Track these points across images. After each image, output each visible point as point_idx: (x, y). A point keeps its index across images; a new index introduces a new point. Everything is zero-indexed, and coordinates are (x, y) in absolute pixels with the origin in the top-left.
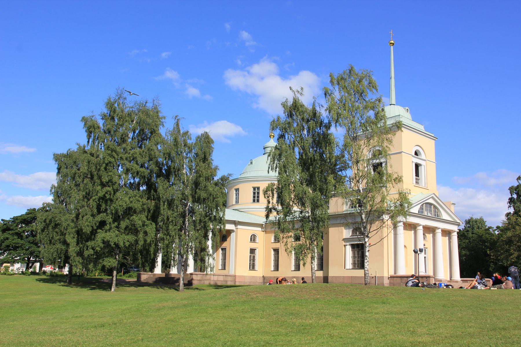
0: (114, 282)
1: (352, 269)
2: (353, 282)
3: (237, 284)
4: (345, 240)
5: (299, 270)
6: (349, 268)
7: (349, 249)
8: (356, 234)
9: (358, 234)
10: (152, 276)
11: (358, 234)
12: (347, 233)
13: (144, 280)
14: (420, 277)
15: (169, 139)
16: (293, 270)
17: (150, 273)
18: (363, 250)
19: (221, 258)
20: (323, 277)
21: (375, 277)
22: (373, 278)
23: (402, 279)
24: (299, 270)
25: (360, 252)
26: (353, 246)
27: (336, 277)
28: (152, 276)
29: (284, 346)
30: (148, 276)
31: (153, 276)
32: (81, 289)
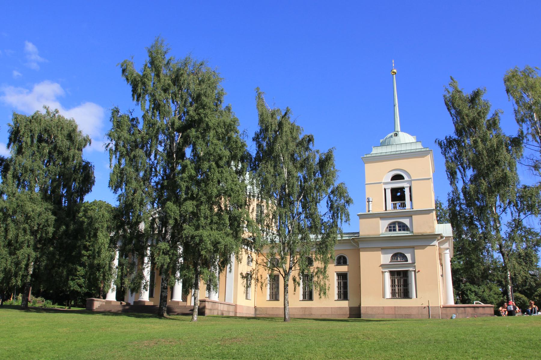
0: (196, 310)
1: (391, 298)
2: (396, 313)
3: (238, 315)
4: (383, 266)
5: (311, 298)
6: (388, 298)
7: (387, 276)
8: (397, 259)
9: (399, 260)
10: (104, 303)
11: (399, 260)
12: (386, 258)
13: (96, 308)
14: (255, 313)
15: (57, 119)
16: (268, 300)
17: (103, 300)
18: (406, 278)
19: (336, 284)
20: (349, 307)
21: (428, 307)
22: (425, 307)
23: (457, 309)
24: (311, 298)
25: (402, 281)
26: (392, 273)
27: (372, 308)
28: (104, 303)
29: (533, 358)
30: (101, 303)
31: (106, 303)
32: (120, 317)
